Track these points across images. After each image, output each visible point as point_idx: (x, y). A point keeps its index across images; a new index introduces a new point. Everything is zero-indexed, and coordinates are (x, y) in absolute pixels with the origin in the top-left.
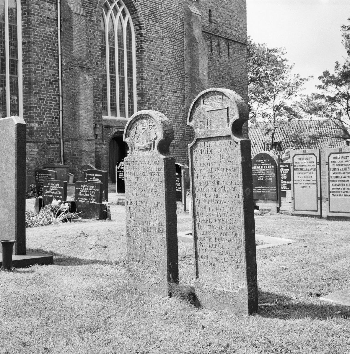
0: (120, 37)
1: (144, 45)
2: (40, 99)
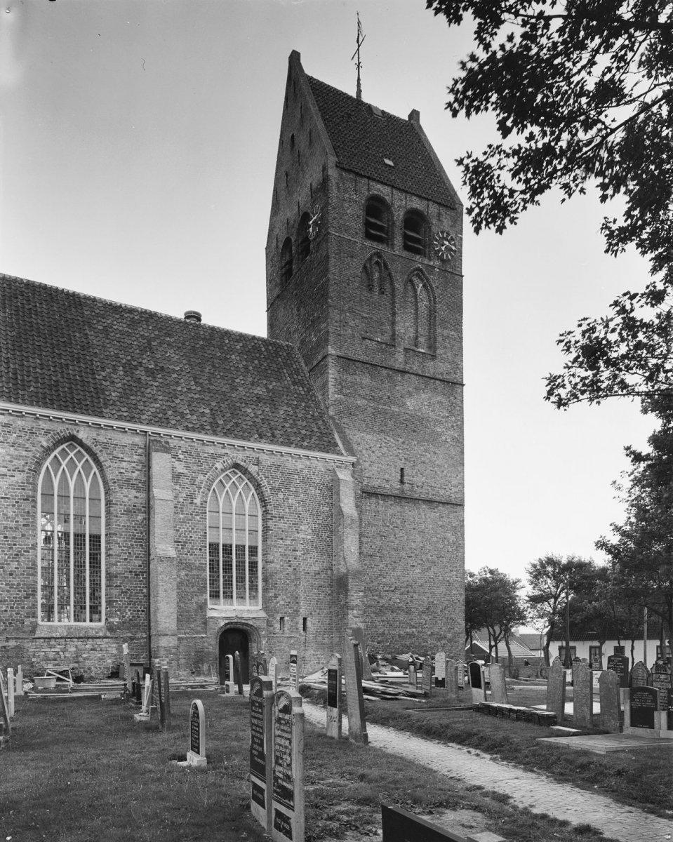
0: (241, 579)
1: (270, 523)
2: (122, 592)
